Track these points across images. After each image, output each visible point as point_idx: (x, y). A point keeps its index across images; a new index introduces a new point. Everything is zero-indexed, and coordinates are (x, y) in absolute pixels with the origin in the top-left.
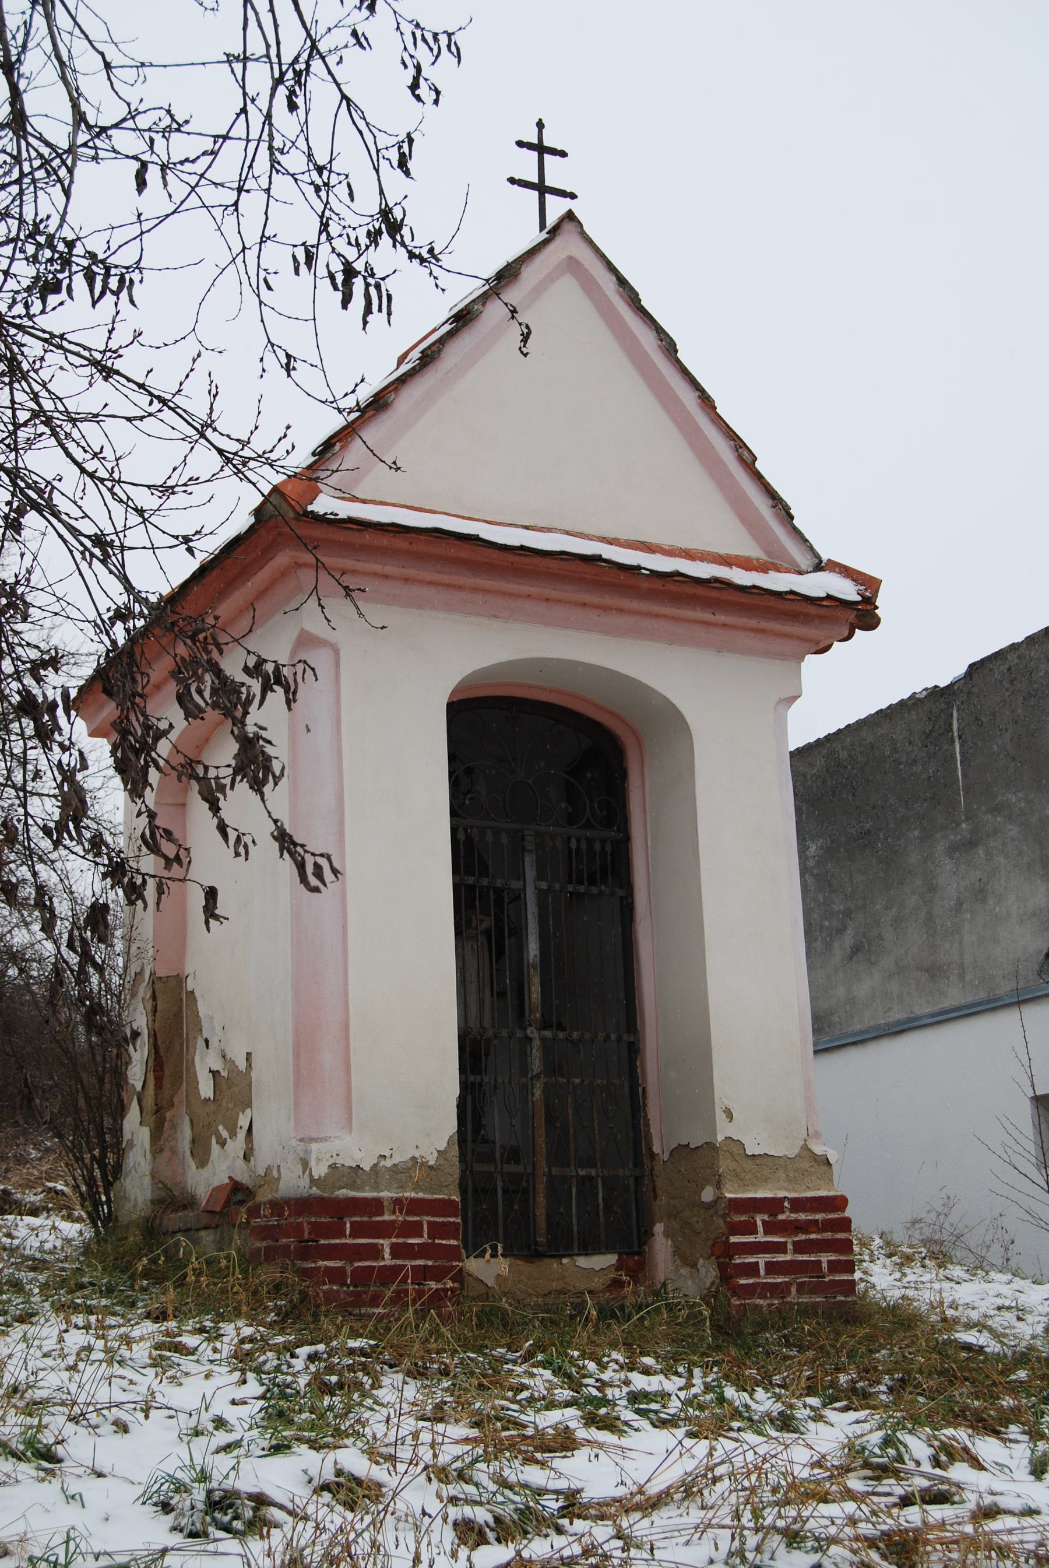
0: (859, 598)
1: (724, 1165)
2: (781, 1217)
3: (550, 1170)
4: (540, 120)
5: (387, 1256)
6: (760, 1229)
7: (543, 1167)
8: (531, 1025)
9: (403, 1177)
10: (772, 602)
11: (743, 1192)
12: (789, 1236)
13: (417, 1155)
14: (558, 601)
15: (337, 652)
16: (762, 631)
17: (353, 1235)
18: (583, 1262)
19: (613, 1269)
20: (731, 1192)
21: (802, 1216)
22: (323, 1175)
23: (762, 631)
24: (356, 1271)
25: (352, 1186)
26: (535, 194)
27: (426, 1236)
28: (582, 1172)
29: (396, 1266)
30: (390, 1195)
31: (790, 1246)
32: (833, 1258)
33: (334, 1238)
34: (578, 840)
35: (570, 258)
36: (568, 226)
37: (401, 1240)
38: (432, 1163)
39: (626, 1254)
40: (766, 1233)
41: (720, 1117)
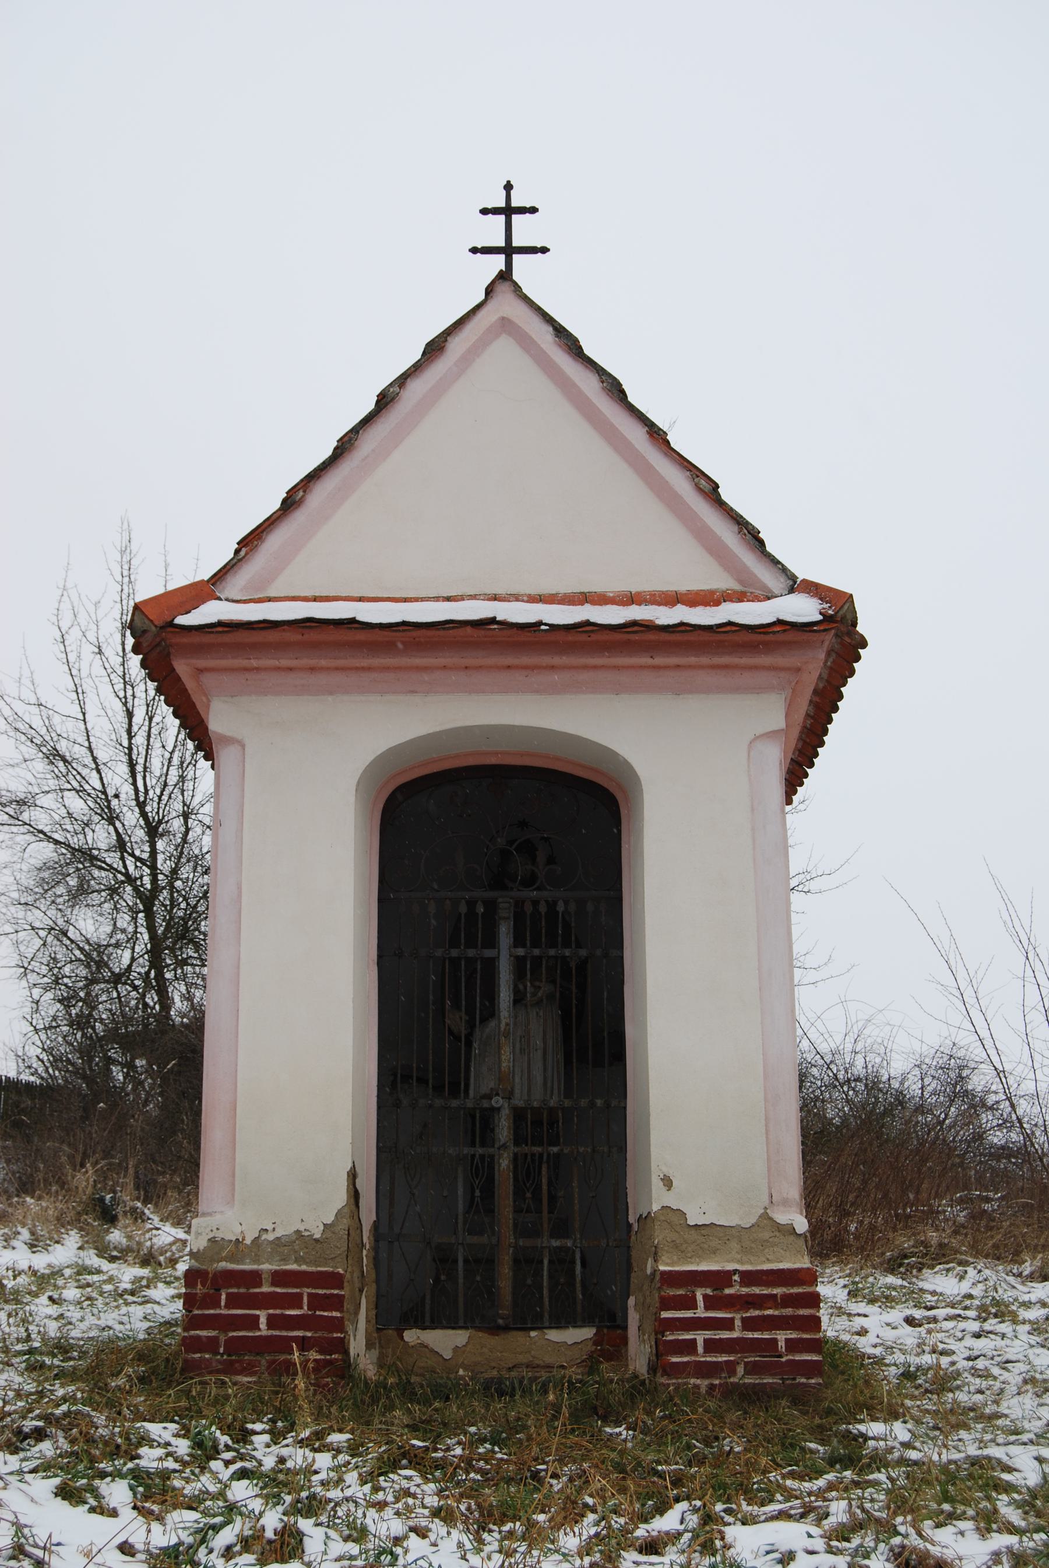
0: (821, 617)
1: (660, 1235)
2: (728, 1291)
4: (509, 182)
7: (508, 1236)
9: (286, 1250)
10: (706, 636)
11: (683, 1264)
12: (737, 1311)
13: (302, 1229)
15: (243, 746)
17: (227, 1306)
19: (590, 1343)
20: (667, 1264)
21: (757, 1290)
22: (202, 1248)
24: (230, 1341)
25: (231, 1258)
27: (306, 1308)
28: (556, 1243)
29: (272, 1336)
30: (270, 1267)
31: (738, 1323)
32: (792, 1336)
33: (209, 1309)
34: (566, 903)
35: (503, 318)
36: (504, 288)
37: (278, 1312)
38: (317, 1236)
39: (608, 1327)
40: (707, 1308)
41: (657, 1184)
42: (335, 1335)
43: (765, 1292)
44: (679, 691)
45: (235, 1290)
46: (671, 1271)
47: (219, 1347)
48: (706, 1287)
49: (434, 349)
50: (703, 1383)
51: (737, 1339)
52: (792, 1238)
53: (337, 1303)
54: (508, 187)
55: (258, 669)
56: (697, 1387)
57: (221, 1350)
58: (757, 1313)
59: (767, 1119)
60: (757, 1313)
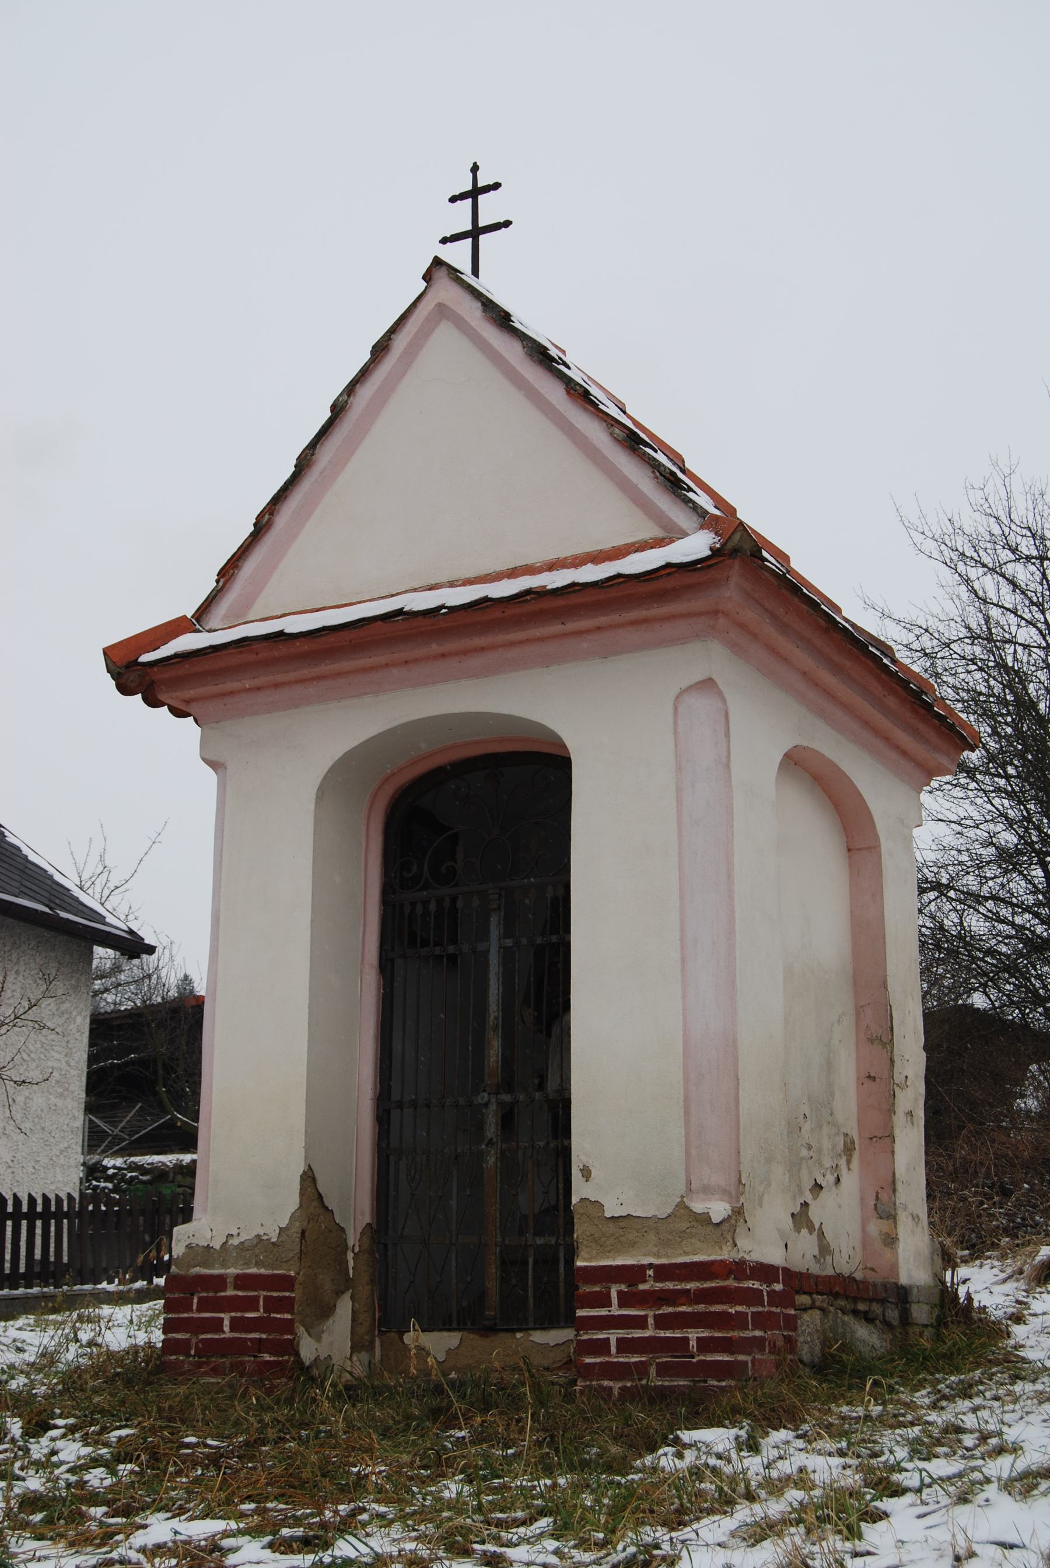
0: (709, 553)
1: (581, 1230)
2: (642, 1287)
3: (504, 1240)
4: (475, 164)
5: (226, 1329)
6: (615, 1300)
8: (484, 1091)
9: (248, 1254)
12: (650, 1308)
14: (417, 660)
16: (645, 621)
17: (199, 1310)
18: (539, 1337)
20: (585, 1260)
21: (670, 1285)
23: (645, 621)
25: (204, 1264)
26: (482, 238)
28: (540, 1241)
37: (239, 1314)
38: (274, 1240)
40: (621, 1305)
42: (286, 1337)
43: (679, 1287)
44: (605, 653)
45: (204, 1294)
46: (586, 1267)
47: (190, 1348)
48: (621, 1283)
49: (380, 349)
50: (616, 1386)
51: (649, 1338)
52: (710, 1228)
53: (286, 1305)
54: (475, 169)
55: (231, 693)
56: (611, 1388)
57: (193, 1352)
58: (671, 1310)
59: (687, 1099)
60: (671, 1310)
